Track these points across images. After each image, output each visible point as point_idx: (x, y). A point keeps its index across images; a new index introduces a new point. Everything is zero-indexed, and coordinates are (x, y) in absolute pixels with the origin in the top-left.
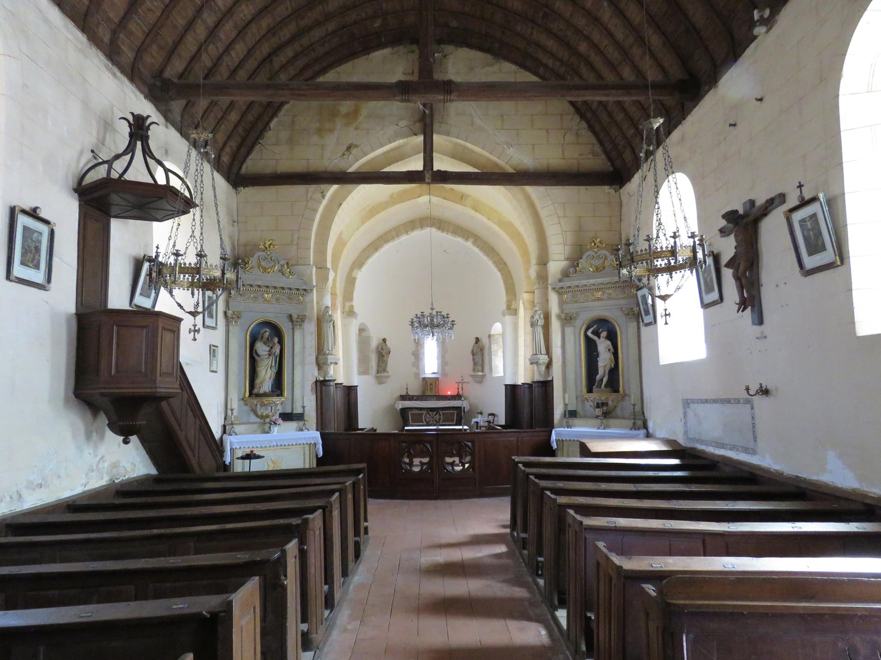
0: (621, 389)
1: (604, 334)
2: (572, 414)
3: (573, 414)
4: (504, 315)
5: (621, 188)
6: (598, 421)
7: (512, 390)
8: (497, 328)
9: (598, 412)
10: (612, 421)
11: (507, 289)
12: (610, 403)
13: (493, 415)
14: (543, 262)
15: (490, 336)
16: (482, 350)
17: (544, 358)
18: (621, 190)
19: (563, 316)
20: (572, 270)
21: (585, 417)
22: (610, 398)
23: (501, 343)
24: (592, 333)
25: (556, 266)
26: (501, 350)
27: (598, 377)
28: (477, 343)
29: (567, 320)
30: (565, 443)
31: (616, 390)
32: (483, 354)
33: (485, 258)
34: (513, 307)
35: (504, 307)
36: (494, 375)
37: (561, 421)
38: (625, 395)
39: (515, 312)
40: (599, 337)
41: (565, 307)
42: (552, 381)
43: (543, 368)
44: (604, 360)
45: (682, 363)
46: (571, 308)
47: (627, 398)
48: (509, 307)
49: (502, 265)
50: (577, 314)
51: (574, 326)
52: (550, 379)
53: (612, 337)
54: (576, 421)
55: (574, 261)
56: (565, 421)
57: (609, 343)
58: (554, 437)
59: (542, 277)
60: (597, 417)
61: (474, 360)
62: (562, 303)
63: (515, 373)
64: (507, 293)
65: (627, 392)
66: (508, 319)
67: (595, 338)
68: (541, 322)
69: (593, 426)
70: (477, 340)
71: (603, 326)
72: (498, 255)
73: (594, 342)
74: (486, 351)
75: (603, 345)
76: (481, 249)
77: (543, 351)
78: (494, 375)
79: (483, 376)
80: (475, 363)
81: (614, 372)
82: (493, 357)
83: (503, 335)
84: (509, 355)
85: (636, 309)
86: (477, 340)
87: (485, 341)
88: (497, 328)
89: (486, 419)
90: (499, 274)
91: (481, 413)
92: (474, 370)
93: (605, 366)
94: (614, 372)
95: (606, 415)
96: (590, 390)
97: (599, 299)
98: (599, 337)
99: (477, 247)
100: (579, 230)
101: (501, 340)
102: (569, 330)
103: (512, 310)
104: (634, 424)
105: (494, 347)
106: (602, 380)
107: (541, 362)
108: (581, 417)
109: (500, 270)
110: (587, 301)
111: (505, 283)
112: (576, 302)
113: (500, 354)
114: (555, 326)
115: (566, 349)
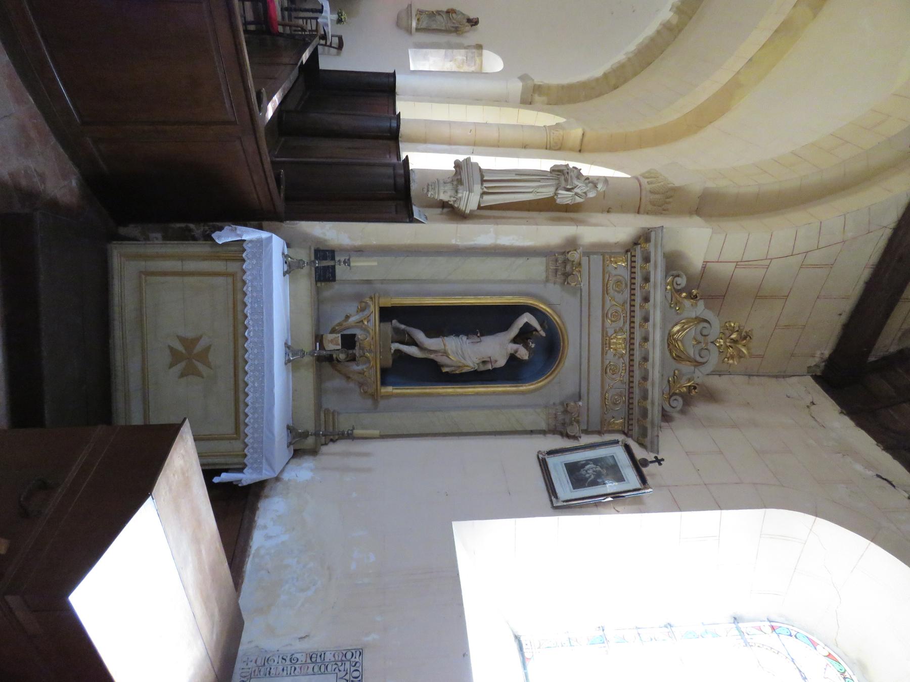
0: (390, 389)
1: (523, 353)
2: (324, 266)
3: (325, 275)
4: (523, 78)
5: (816, 378)
6: (307, 344)
7: (383, 88)
8: (493, 63)
9: (333, 343)
10: (308, 376)
11: (570, 88)
12: (355, 367)
13: (340, 46)
14: (709, 206)
15: (479, 47)
16: (456, 30)
17: (470, 200)
18: (809, 380)
19: (575, 256)
20: (682, 281)
21: (318, 302)
22: (368, 367)
23: (466, 68)
24: (527, 325)
25: (698, 242)
26: (455, 69)
27: (420, 336)
28: (469, 21)
29: (564, 263)
30: (232, 267)
31: (387, 375)
32: (447, 31)
33: (632, 47)
34: (537, 98)
35: (538, 80)
36: (411, 52)
37: (306, 238)
38: (375, 397)
39: (526, 101)
40: (515, 340)
41: (597, 260)
42: (411, 219)
43: (444, 197)
44: (460, 351)
45: (465, 655)
46: (591, 277)
47: (369, 402)
48: (538, 89)
49: (616, 79)
50: (577, 291)
51: (547, 280)
52: (417, 212)
53: (513, 371)
54: (305, 283)
55: (699, 288)
56: (304, 255)
57: (502, 362)
58: (250, 234)
59: (666, 200)
60: (319, 338)
61: (439, 13)
62: (603, 251)
63: (419, 96)
64: (563, 87)
65: (382, 403)
66: (516, 87)
67: (514, 331)
68: (565, 197)
69: (293, 327)
70: (474, 22)
71: (545, 347)
72: (635, 74)
73: (506, 327)
74: (453, 38)
75: (496, 348)
76: (652, 40)
77: (490, 200)
78: (411, 52)
79: (409, 30)
80: (432, 15)
81: (432, 372)
82: (442, 52)
83: (480, 74)
84: (449, 85)
85: (573, 430)
86: (474, 22)
87: (472, 37)
88: (493, 63)
89: (330, 31)
90: (598, 73)
91: (340, 21)
92: (420, 12)
93: (445, 353)
94: (432, 372)
95: (325, 360)
96: (387, 314)
97: (606, 343)
98: (515, 340)
99: (658, 32)
100: (759, 295)
101: (472, 69)
102: (538, 268)
103: (533, 94)
104: (305, 435)
105: (460, 55)
106: (413, 342)
107: (463, 194)
108: (318, 291)
109: (606, 75)
110: (605, 316)
111: (584, 85)
112: (605, 291)
113: (448, 66)
114: (549, 233)
115: (488, 257)
